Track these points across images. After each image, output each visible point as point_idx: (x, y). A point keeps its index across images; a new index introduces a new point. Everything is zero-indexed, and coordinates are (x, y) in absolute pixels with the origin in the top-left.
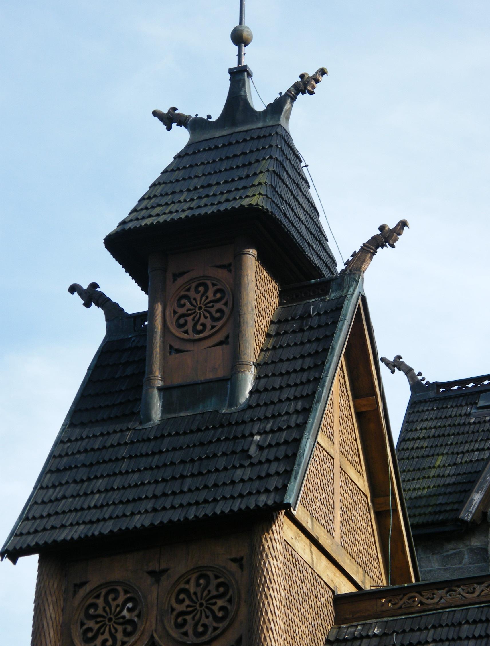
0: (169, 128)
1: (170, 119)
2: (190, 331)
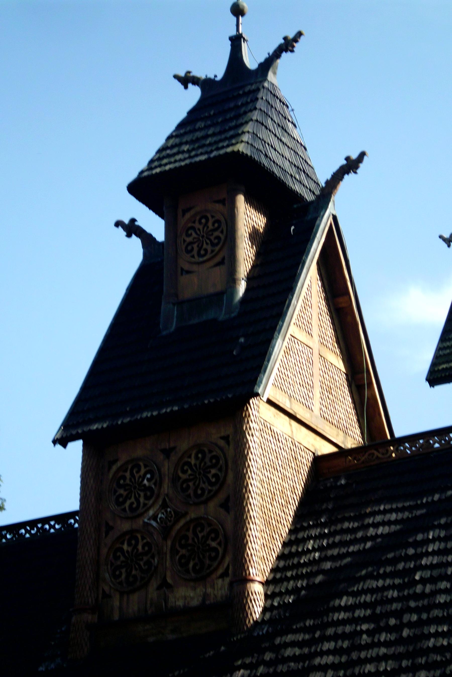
0: (186, 87)
1: (186, 80)
2: (196, 256)
